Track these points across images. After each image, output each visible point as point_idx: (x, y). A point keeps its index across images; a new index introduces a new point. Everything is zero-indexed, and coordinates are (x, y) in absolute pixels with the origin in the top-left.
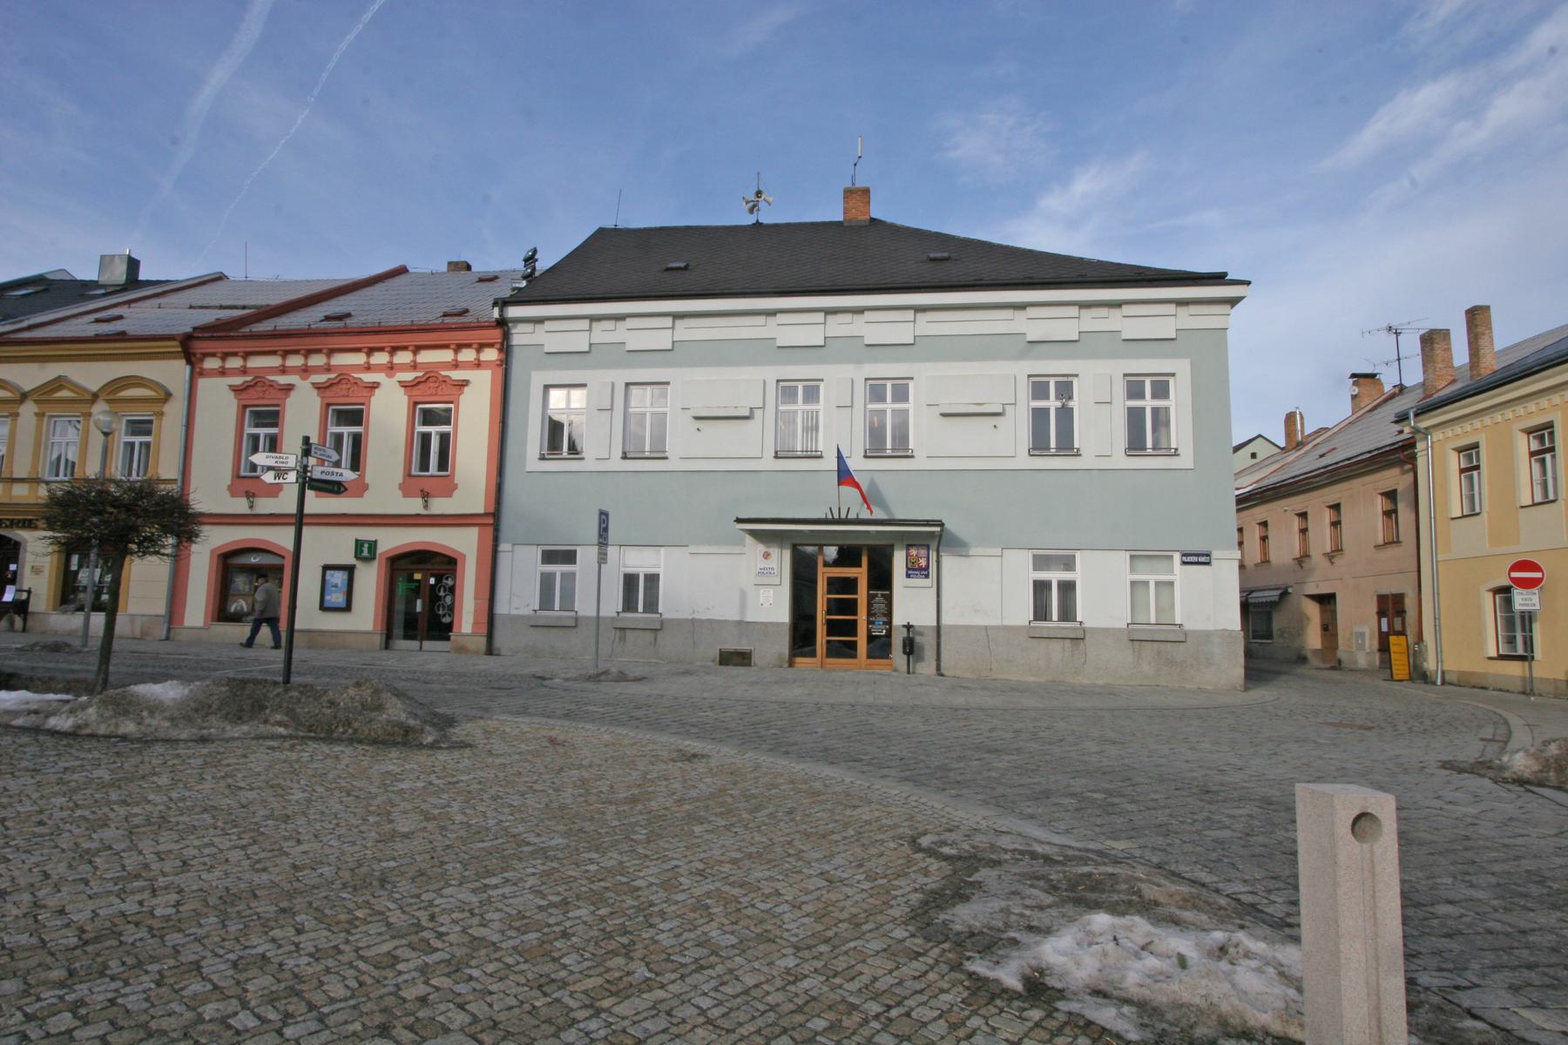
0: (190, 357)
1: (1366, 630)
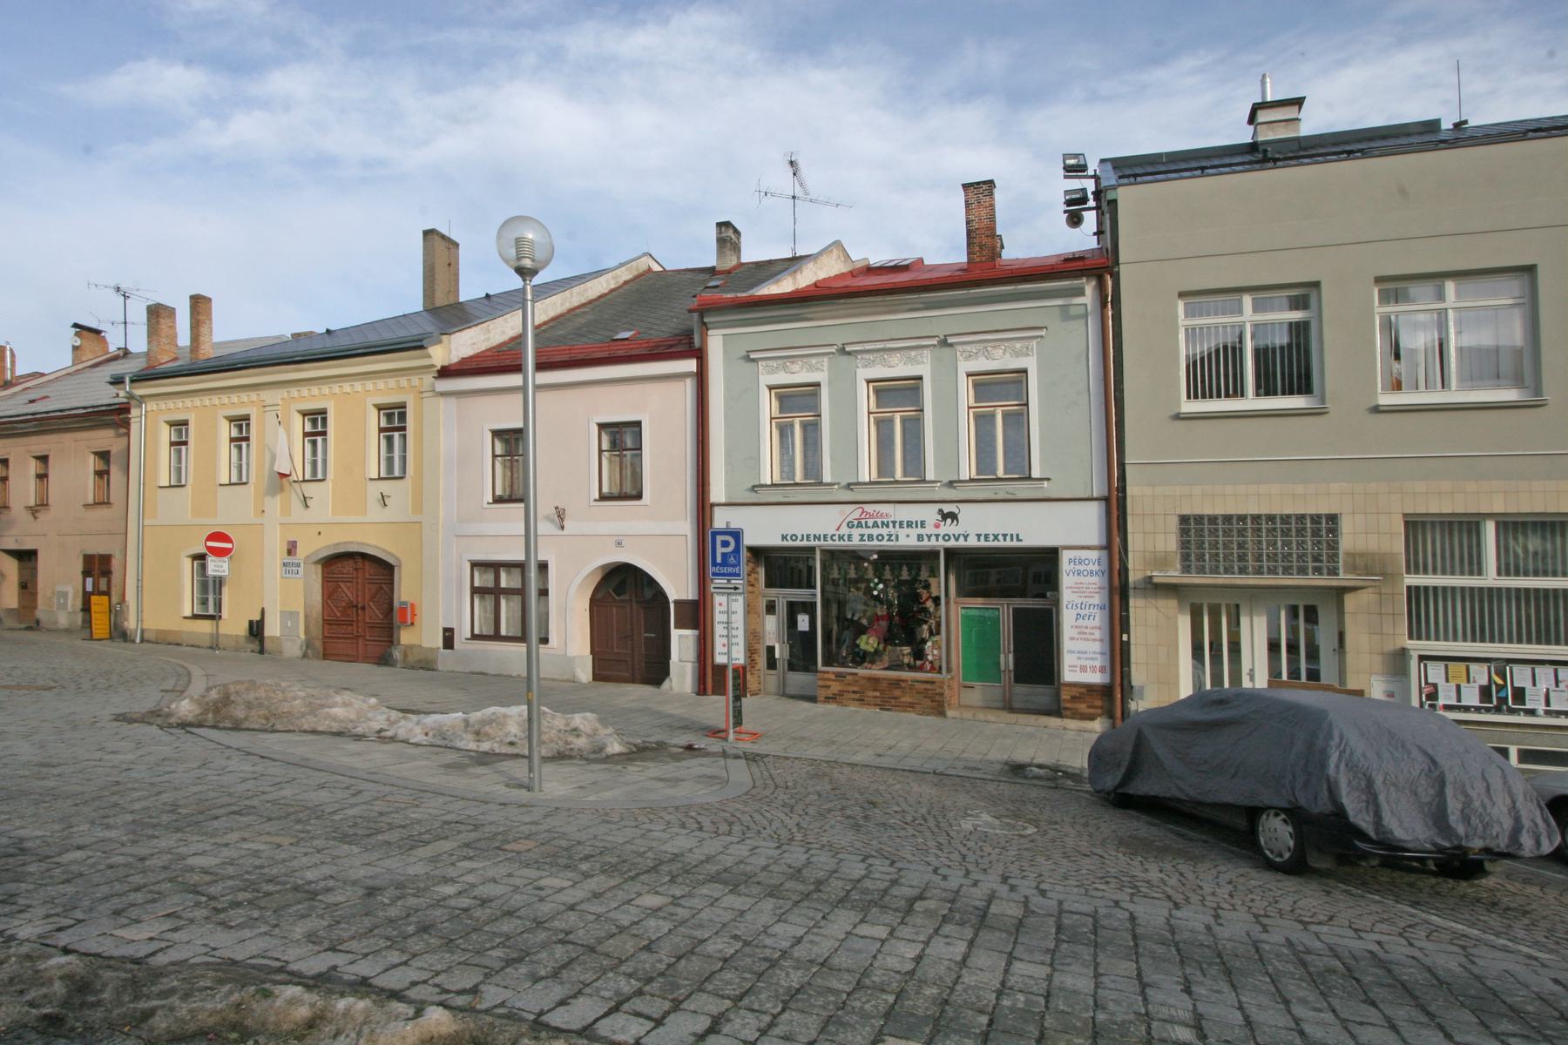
1: (70, 590)
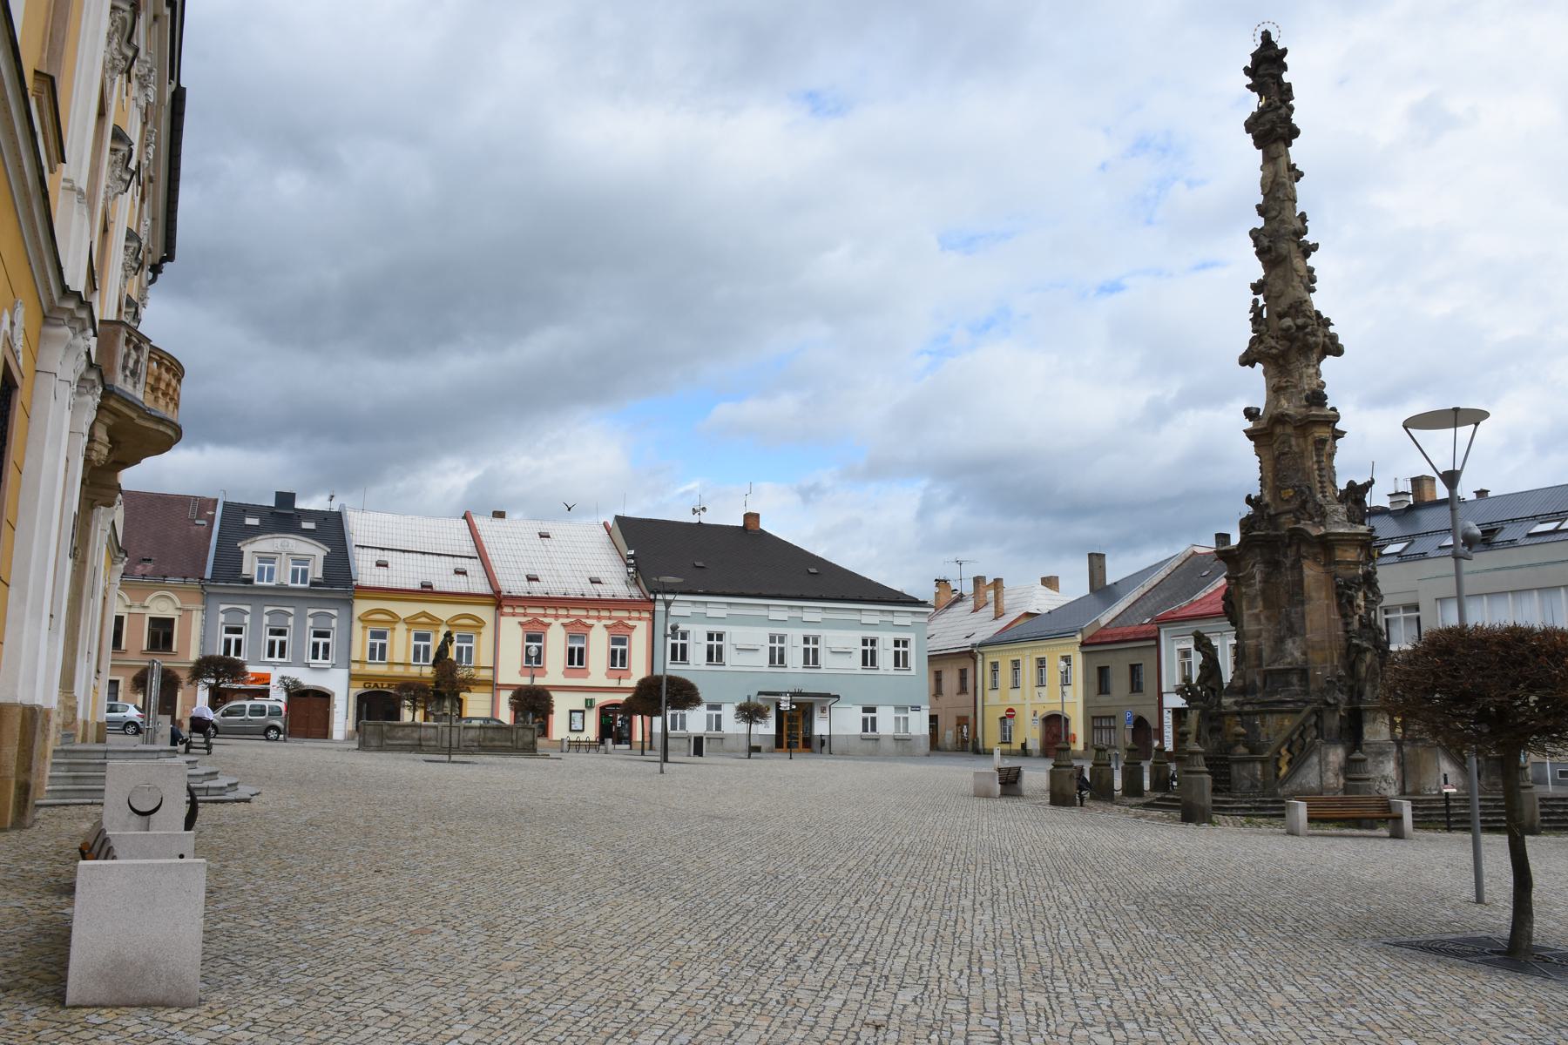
0: (499, 606)
